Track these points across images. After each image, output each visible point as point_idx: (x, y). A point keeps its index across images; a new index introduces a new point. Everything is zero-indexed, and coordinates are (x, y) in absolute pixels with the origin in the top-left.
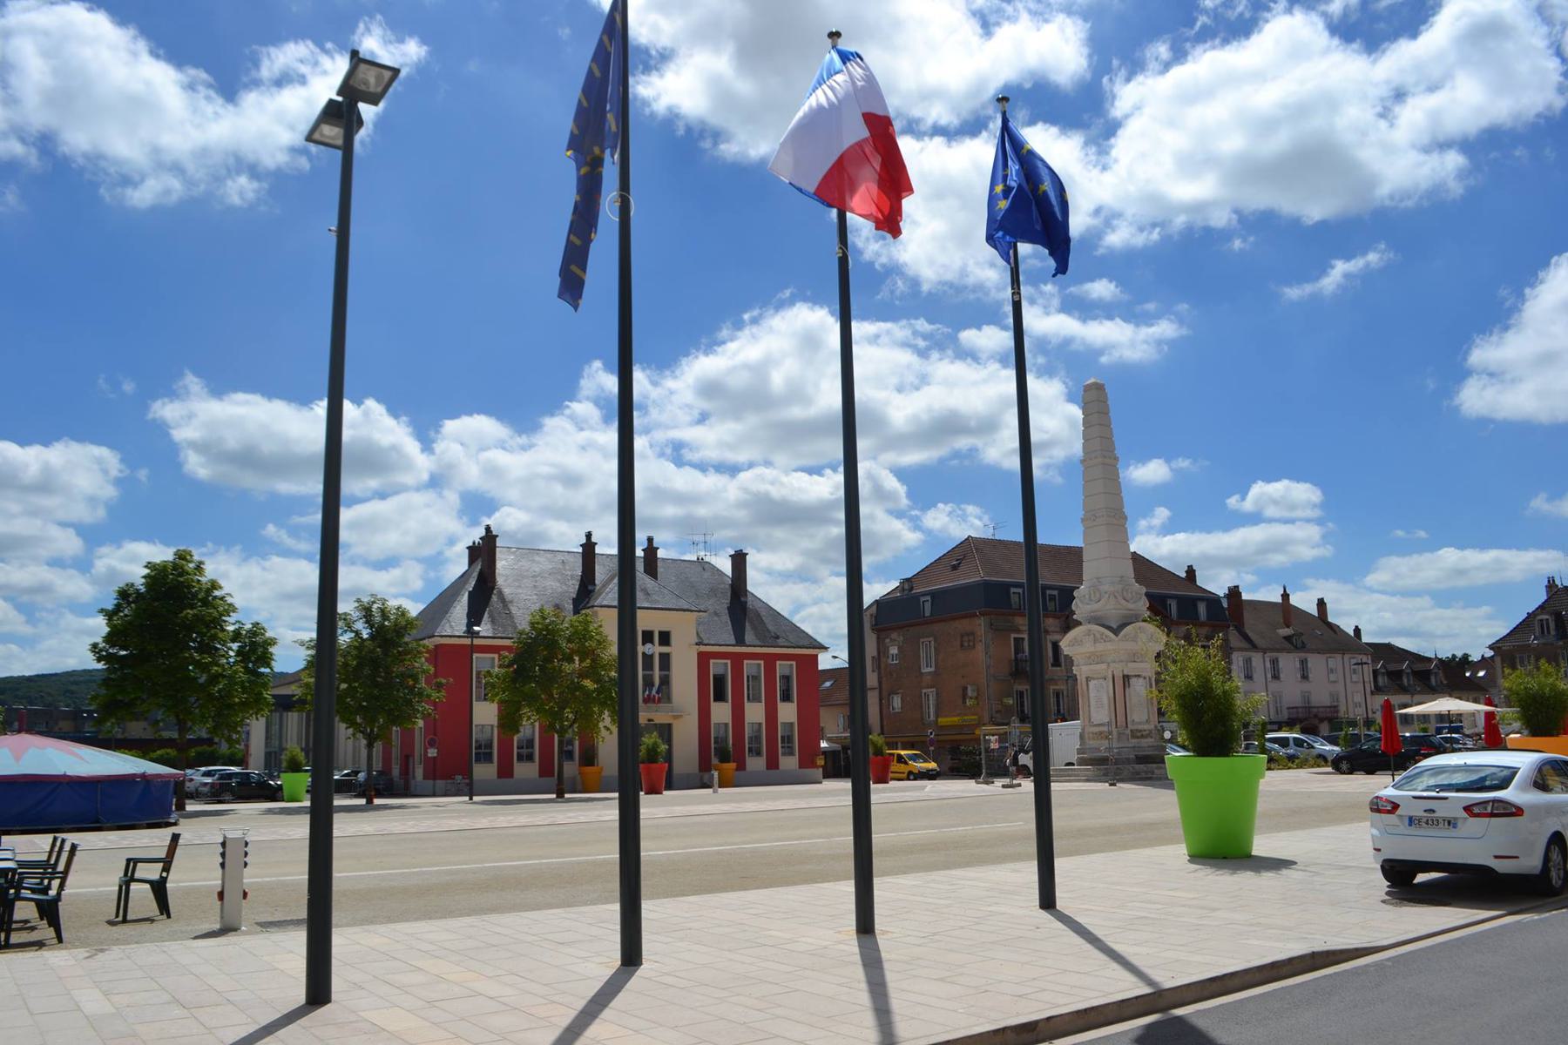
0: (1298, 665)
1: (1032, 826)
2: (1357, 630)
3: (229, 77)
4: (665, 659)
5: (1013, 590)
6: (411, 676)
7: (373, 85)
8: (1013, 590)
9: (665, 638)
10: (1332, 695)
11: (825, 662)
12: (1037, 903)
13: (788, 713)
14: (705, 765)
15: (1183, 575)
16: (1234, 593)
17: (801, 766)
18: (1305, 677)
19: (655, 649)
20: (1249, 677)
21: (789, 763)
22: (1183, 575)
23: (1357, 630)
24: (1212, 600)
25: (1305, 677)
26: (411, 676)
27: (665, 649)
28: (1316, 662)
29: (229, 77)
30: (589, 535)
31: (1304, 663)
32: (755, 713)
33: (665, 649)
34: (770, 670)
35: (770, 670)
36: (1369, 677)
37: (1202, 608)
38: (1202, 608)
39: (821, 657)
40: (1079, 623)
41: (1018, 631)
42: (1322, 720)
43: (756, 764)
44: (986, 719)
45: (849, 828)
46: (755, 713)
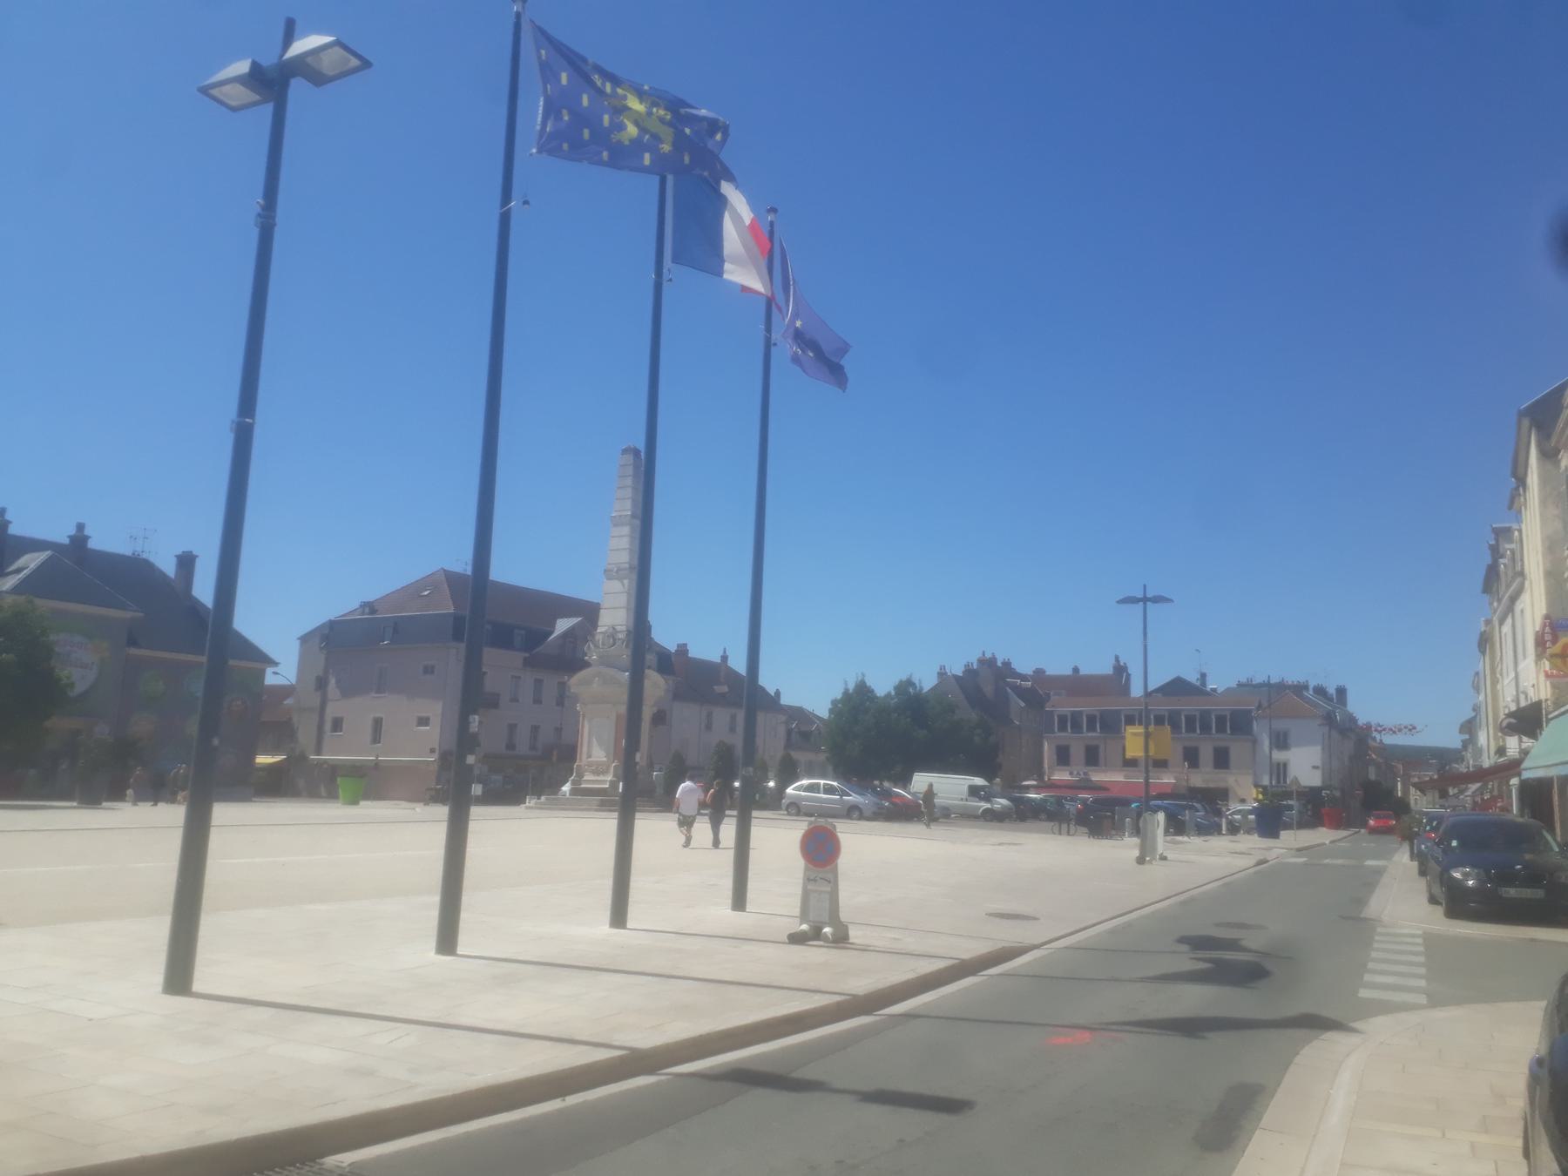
1: (209, 925)
2: (778, 693)
11: (270, 679)
16: (682, 650)
23: (778, 693)
36: (782, 731)
39: (269, 671)
40: (587, 665)
45: (753, 843)
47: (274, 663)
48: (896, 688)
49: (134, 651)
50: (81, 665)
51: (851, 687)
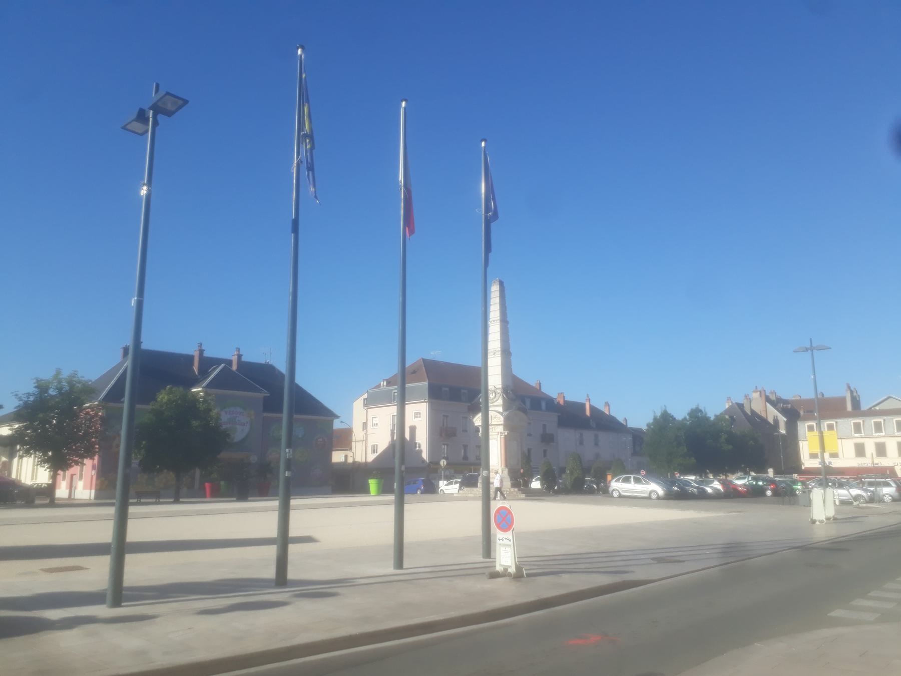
5: (444, 389)
7: (170, 107)
8: (444, 389)
12: (392, 566)
18: (596, 444)
24: (550, 402)
25: (596, 444)
28: (603, 436)
30: (238, 349)
37: (543, 404)
38: (543, 404)
47: (337, 417)
48: (689, 414)
49: (265, 414)
50: (238, 420)
51: (658, 414)
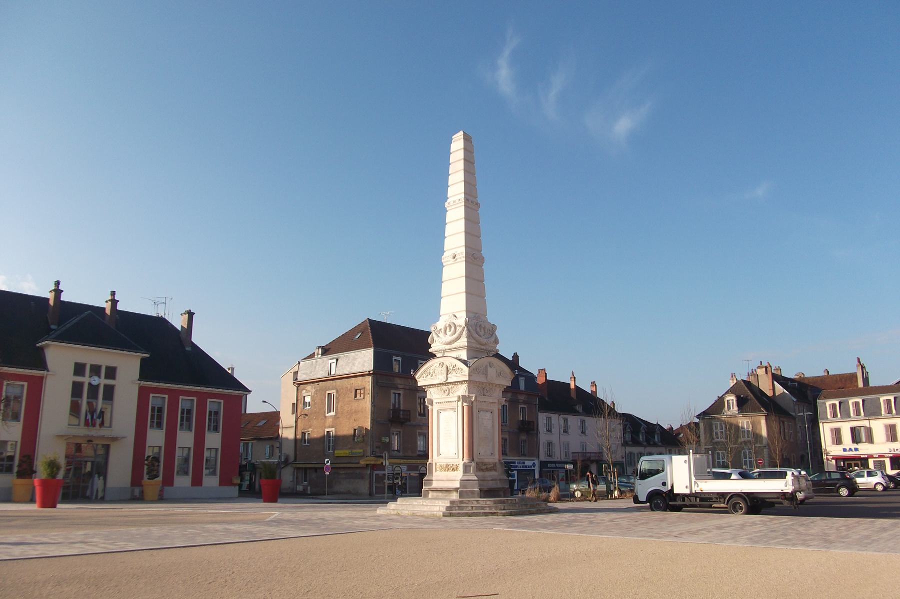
0: (579, 423)
3: (892, 469)
4: (109, 392)
6: (600, 472)
9: (111, 373)
10: (599, 445)
13: (213, 440)
14: (136, 480)
15: (511, 359)
17: (221, 484)
19: (101, 381)
20: (549, 431)
21: (211, 481)
22: (511, 359)
26: (600, 472)
27: (110, 382)
29: (892, 469)
30: (57, 283)
31: (583, 422)
32: (185, 439)
33: (110, 382)
34: (173, 404)
35: (173, 404)
41: (397, 388)
42: (592, 462)
43: (182, 482)
44: (369, 454)
46: (185, 439)
